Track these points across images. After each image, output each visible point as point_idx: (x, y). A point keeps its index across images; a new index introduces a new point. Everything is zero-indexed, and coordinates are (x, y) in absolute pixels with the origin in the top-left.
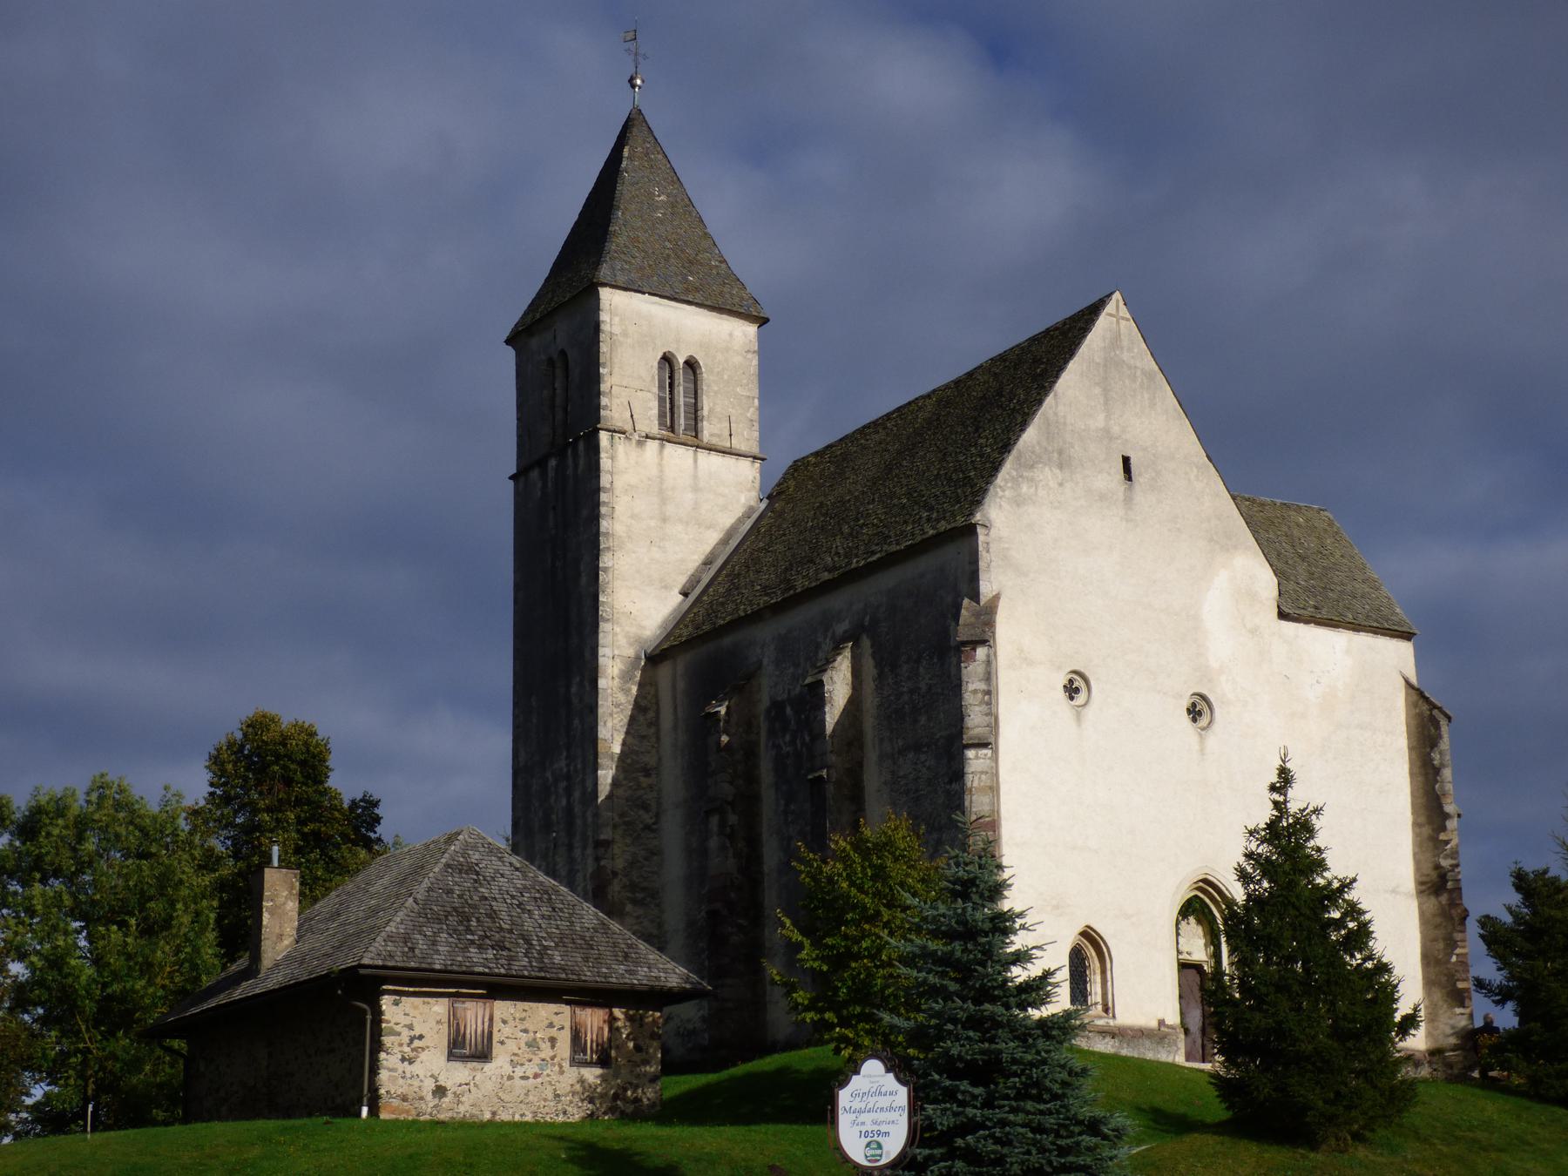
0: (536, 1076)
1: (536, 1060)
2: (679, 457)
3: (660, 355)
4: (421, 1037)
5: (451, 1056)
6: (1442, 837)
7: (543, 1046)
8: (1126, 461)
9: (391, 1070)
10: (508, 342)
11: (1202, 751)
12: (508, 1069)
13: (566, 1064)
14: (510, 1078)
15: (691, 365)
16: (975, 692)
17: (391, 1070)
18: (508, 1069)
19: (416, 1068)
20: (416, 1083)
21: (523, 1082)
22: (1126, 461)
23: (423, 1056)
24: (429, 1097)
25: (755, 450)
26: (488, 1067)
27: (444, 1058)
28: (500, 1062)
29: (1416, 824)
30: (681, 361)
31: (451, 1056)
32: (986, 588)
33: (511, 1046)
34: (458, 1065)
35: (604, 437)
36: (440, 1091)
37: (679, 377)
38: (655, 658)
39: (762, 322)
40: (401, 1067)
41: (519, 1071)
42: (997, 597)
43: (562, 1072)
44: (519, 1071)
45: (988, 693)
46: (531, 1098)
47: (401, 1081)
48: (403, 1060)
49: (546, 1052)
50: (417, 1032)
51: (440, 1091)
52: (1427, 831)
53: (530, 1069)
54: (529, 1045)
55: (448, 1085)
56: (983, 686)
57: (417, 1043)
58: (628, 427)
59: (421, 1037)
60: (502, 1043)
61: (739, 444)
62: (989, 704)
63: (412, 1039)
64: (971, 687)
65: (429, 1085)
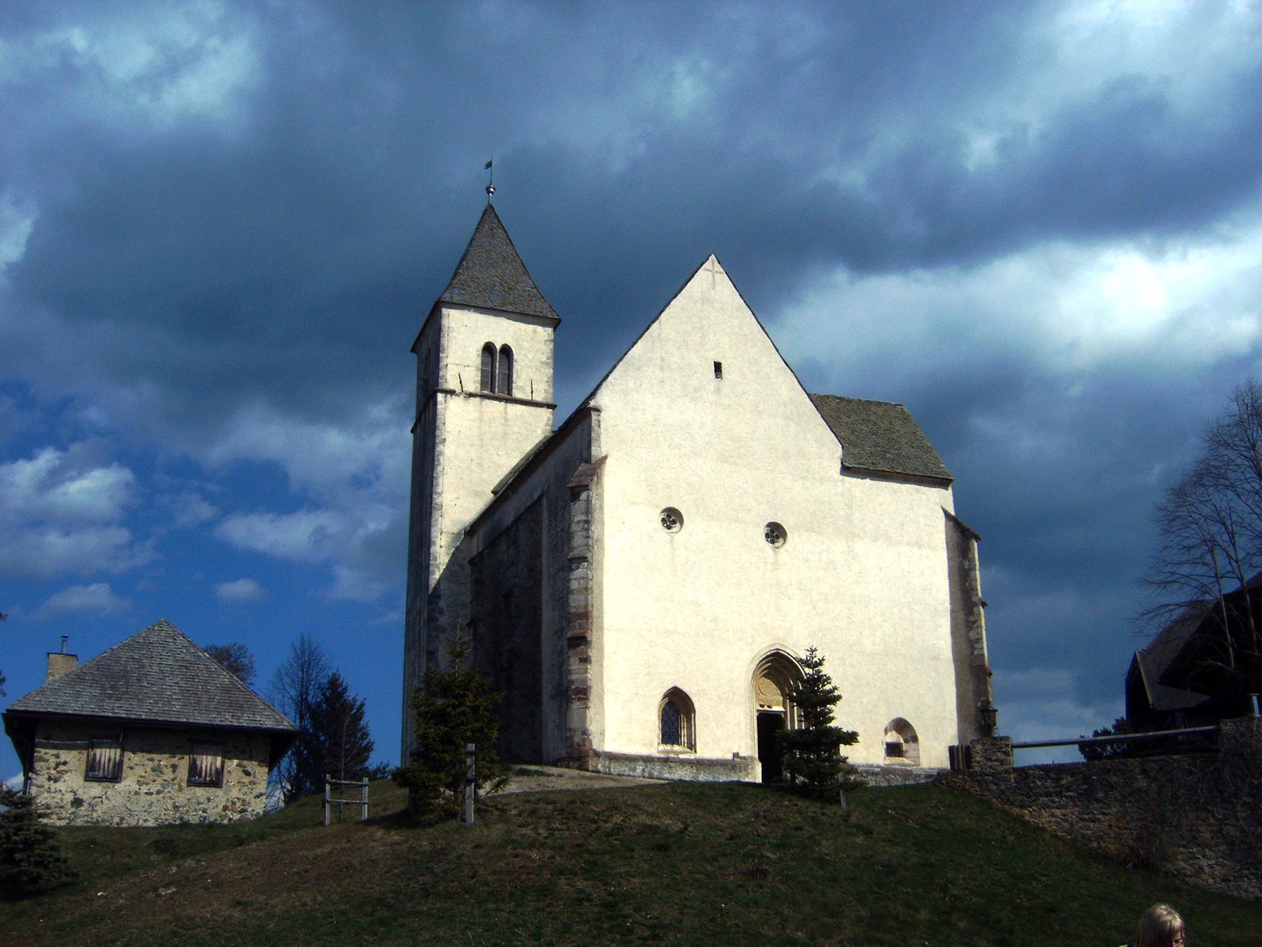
0: (158, 792)
1: (159, 780)
2: (494, 407)
3: (482, 344)
4: (65, 763)
5: (88, 778)
6: (972, 619)
7: (165, 770)
8: (718, 367)
9: (38, 786)
10: (413, 350)
11: (671, 542)
12: (135, 787)
13: (184, 784)
14: (136, 793)
15: (506, 351)
16: (579, 522)
17: (38, 786)
18: (135, 787)
19: (60, 785)
20: (59, 796)
21: (148, 797)
22: (718, 367)
23: (66, 777)
24: (69, 806)
25: (550, 401)
26: (117, 786)
27: (82, 778)
28: (128, 783)
29: (952, 612)
30: (498, 347)
31: (88, 778)
32: (596, 452)
33: (139, 771)
34: (95, 784)
35: (440, 397)
36: (77, 802)
37: (497, 362)
38: (471, 531)
39: (555, 324)
40: (47, 784)
41: (144, 789)
42: (605, 458)
43: (181, 789)
44: (144, 789)
45: (587, 522)
46: (154, 808)
47: (46, 795)
48: (49, 779)
49: (168, 774)
50: (62, 760)
51: (77, 802)
52: (961, 615)
53: (154, 788)
54: (153, 770)
55: (85, 797)
56: (583, 518)
57: (61, 768)
58: (458, 390)
59: (65, 763)
60: (131, 768)
61: (539, 397)
62: (587, 530)
63: (58, 765)
64: (577, 519)
65: (70, 797)
